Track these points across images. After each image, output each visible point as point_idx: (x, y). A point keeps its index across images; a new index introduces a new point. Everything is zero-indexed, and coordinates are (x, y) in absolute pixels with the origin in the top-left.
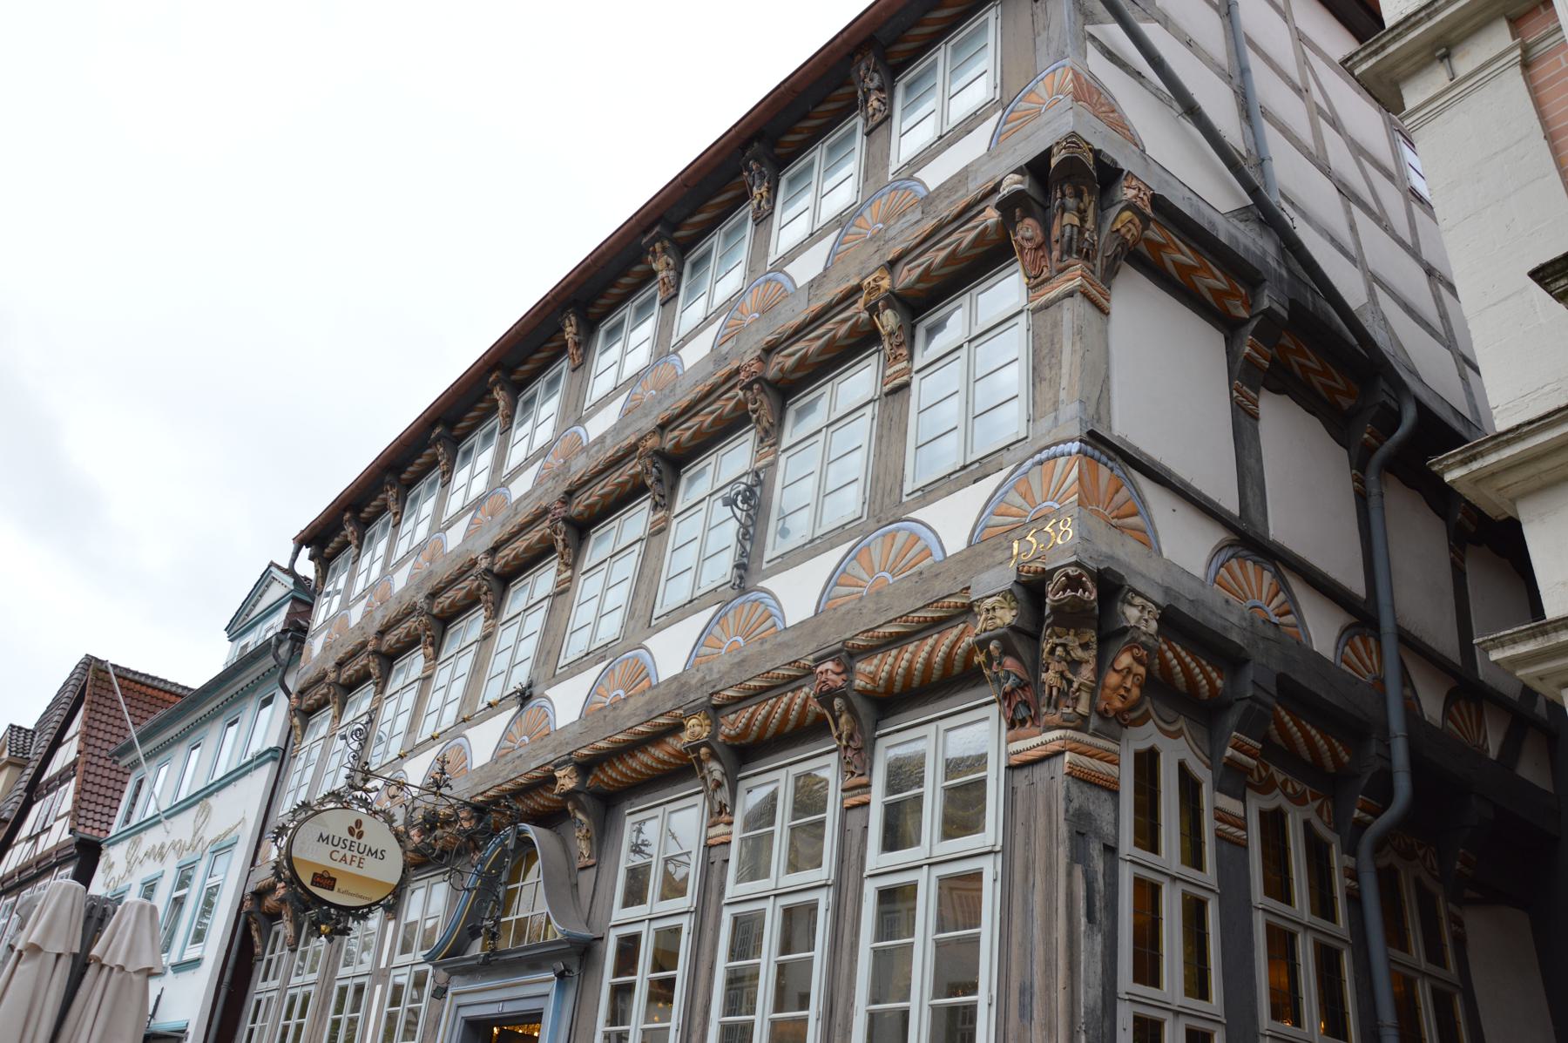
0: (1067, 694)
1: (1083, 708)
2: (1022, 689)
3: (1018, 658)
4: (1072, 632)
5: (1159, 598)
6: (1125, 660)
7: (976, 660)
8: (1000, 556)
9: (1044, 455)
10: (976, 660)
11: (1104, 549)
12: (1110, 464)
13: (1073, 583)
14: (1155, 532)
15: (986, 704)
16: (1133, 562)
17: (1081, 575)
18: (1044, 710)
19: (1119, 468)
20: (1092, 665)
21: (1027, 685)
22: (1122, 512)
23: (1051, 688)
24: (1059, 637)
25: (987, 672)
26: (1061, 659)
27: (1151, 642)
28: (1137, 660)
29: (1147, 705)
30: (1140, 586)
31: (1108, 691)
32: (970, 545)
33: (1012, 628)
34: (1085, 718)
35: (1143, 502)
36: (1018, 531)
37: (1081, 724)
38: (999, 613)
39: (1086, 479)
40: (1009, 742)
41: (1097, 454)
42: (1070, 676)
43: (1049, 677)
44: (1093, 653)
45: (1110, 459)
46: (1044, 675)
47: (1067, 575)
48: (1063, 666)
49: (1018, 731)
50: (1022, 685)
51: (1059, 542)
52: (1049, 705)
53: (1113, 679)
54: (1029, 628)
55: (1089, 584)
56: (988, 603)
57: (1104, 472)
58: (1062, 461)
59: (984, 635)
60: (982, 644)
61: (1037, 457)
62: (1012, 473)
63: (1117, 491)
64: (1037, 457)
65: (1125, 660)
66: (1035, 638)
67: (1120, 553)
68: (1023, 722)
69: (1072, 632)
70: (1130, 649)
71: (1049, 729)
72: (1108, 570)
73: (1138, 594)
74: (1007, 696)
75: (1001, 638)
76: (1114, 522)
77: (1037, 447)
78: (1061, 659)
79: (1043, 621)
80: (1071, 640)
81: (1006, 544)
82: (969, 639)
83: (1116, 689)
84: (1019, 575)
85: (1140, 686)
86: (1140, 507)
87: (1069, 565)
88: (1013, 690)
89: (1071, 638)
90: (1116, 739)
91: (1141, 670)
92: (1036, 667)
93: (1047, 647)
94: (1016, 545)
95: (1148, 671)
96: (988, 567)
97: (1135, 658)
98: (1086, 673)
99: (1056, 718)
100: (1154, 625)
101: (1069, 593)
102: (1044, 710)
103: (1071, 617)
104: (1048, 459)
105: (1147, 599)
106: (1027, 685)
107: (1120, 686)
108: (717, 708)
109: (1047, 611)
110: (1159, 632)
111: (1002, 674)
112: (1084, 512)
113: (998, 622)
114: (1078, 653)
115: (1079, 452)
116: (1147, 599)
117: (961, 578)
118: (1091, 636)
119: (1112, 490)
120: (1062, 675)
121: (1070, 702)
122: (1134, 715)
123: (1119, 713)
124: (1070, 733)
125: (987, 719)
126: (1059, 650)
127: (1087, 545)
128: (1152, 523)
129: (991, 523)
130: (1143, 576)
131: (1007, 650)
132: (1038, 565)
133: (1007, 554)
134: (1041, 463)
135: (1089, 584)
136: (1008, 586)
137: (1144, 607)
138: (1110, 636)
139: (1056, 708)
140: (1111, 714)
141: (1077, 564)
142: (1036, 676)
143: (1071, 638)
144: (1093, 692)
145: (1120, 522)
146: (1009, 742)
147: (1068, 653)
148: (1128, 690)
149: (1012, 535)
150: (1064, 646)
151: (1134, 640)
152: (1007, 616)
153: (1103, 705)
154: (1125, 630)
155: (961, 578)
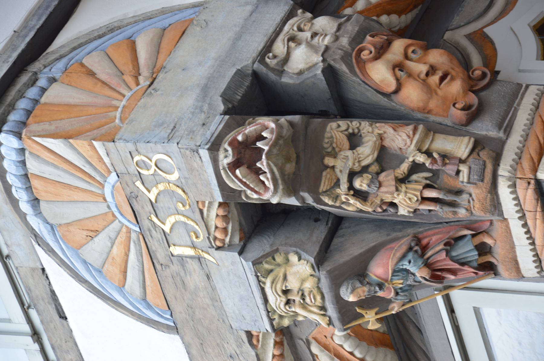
0: (436, 173)
1: (461, 147)
2: (425, 249)
3: (371, 254)
4: (329, 161)
5: (277, 12)
6: (380, 73)
7: (374, 325)
8: (195, 278)
9: (21, 196)
10: (374, 325)
11: (189, 101)
12: (42, 82)
13: (246, 156)
14: (164, 12)
15: (451, 311)
16: (213, 53)
17: (234, 143)
18: (462, 213)
19: (45, 68)
20: (386, 129)
21: (418, 241)
22: (128, 68)
23: (424, 200)
24: (337, 184)
25: (395, 308)
26: (375, 180)
27: (351, 28)
28: (381, 51)
29: (459, 36)
30: (256, 43)
31: (433, 104)
32: (175, 329)
33: (320, 261)
34: (478, 145)
35: (111, 30)
36: (154, 245)
37: (488, 151)
38: (293, 284)
39: (66, 125)
40: (519, 275)
41: (23, 104)
42: (404, 167)
43: (406, 202)
44: (365, 126)
45: (33, 82)
46: (403, 211)
47: (234, 166)
48: (388, 178)
49: (498, 257)
50: (419, 248)
51: (174, 177)
52: (452, 204)
53: (412, 95)
54: (320, 232)
55: (250, 129)
56: (276, 301)
57: (57, 94)
58: (33, 166)
59: (332, 311)
60: (347, 314)
61: (25, 207)
62: (51, 251)
63: (91, 74)
64: (25, 207)
65: (380, 73)
66: (337, 223)
67: (199, 73)
68: (483, 249)
69: (329, 161)
70: (362, 64)
71: (496, 205)
72: (226, 97)
73: (268, 47)
74: (436, 275)
75: (336, 282)
76: (144, 82)
77: (7, 208)
78: (375, 180)
79: (311, 209)
80: (343, 162)
81: (175, 268)
82: (338, 337)
83: (429, 90)
84: (230, 247)
85: (427, 48)
86: (119, 36)
87: (215, 161)
88: (427, 265)
89: (339, 164)
90: (517, 91)
91: (399, 46)
92: (387, 223)
93: (354, 205)
94: (176, 251)
95: (401, 33)
96: (215, 299)
97: (378, 57)
98: (401, 140)
99: (477, 193)
100: (323, 22)
101: (263, 164)
102: (462, 213)
103: (304, 162)
104: (29, 189)
105: (277, 33)
106: (418, 241)
107: (424, 82)
108: (199, 259)
109: (293, 201)
110: (335, 14)
111: (399, 283)
112: (125, 131)
113: (308, 285)
114: (367, 152)
115: (19, 135)
116: (277, 33)
117: (231, 347)
118: (336, 130)
119: (88, 82)
120: (403, 180)
121: (450, 169)
122: (476, 60)
123: (472, 86)
124: (504, 171)
125: (477, 312)
126: (358, 184)
127: (182, 131)
128: (148, 17)
129: (138, 291)
130: (238, 37)
131: (358, 272)
132: (214, 215)
133: (193, 265)
134: (35, 202)
135: (250, 129)
136: (248, 266)
137: (292, 39)
138: (339, 100)
139: (459, 192)
140: (473, 99)
141: (214, 147)
142: (404, 224)
143: (339, 164)
144: (434, 130)
145: (145, 72)
146: (519, 275)
147: (365, 169)
148: (432, 70)
149: (160, 255)
150: (352, 175)
151: (346, 58)
152: (299, 270)
153: (457, 114)
154: (330, 72)
155: (231, 347)
